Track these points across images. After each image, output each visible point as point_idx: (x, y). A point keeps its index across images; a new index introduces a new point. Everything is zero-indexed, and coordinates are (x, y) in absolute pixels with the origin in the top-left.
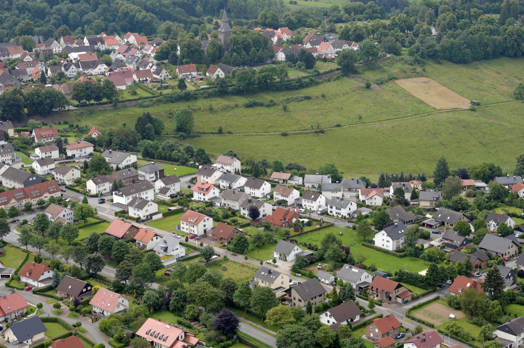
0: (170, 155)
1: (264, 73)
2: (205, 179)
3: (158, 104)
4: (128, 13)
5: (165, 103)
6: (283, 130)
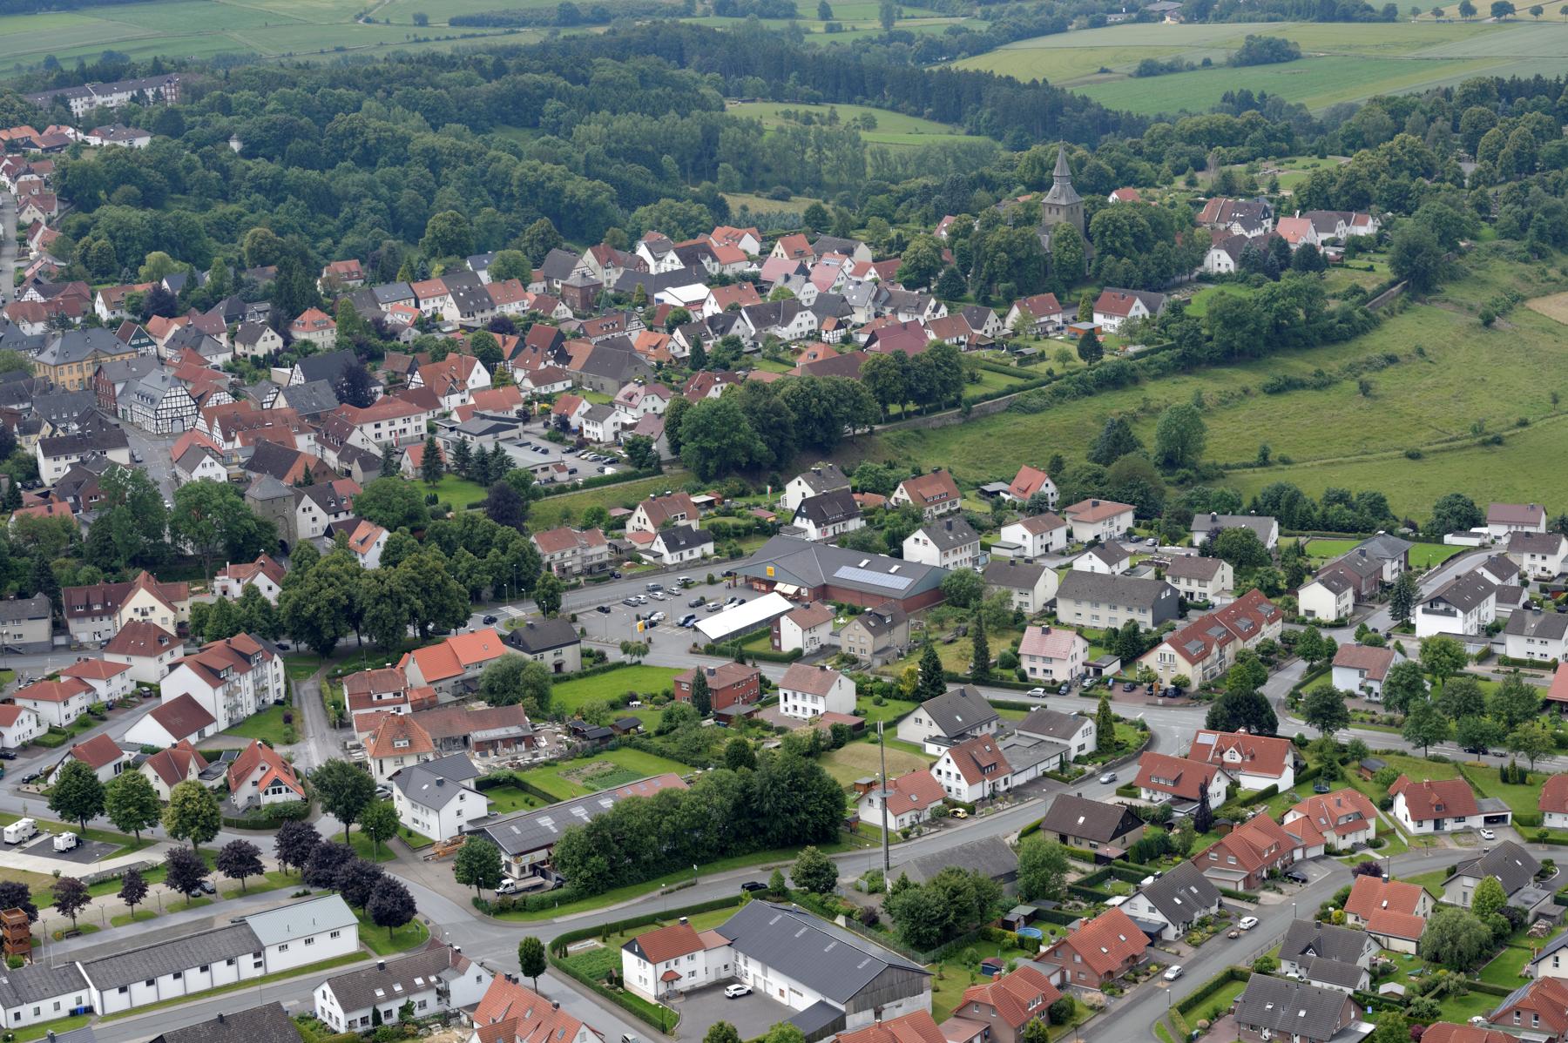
0: (1324, 516)
1: (1281, 302)
2: (1538, 560)
3: (1060, 403)
4: (540, 185)
5: (1075, 398)
6: (1412, 444)
